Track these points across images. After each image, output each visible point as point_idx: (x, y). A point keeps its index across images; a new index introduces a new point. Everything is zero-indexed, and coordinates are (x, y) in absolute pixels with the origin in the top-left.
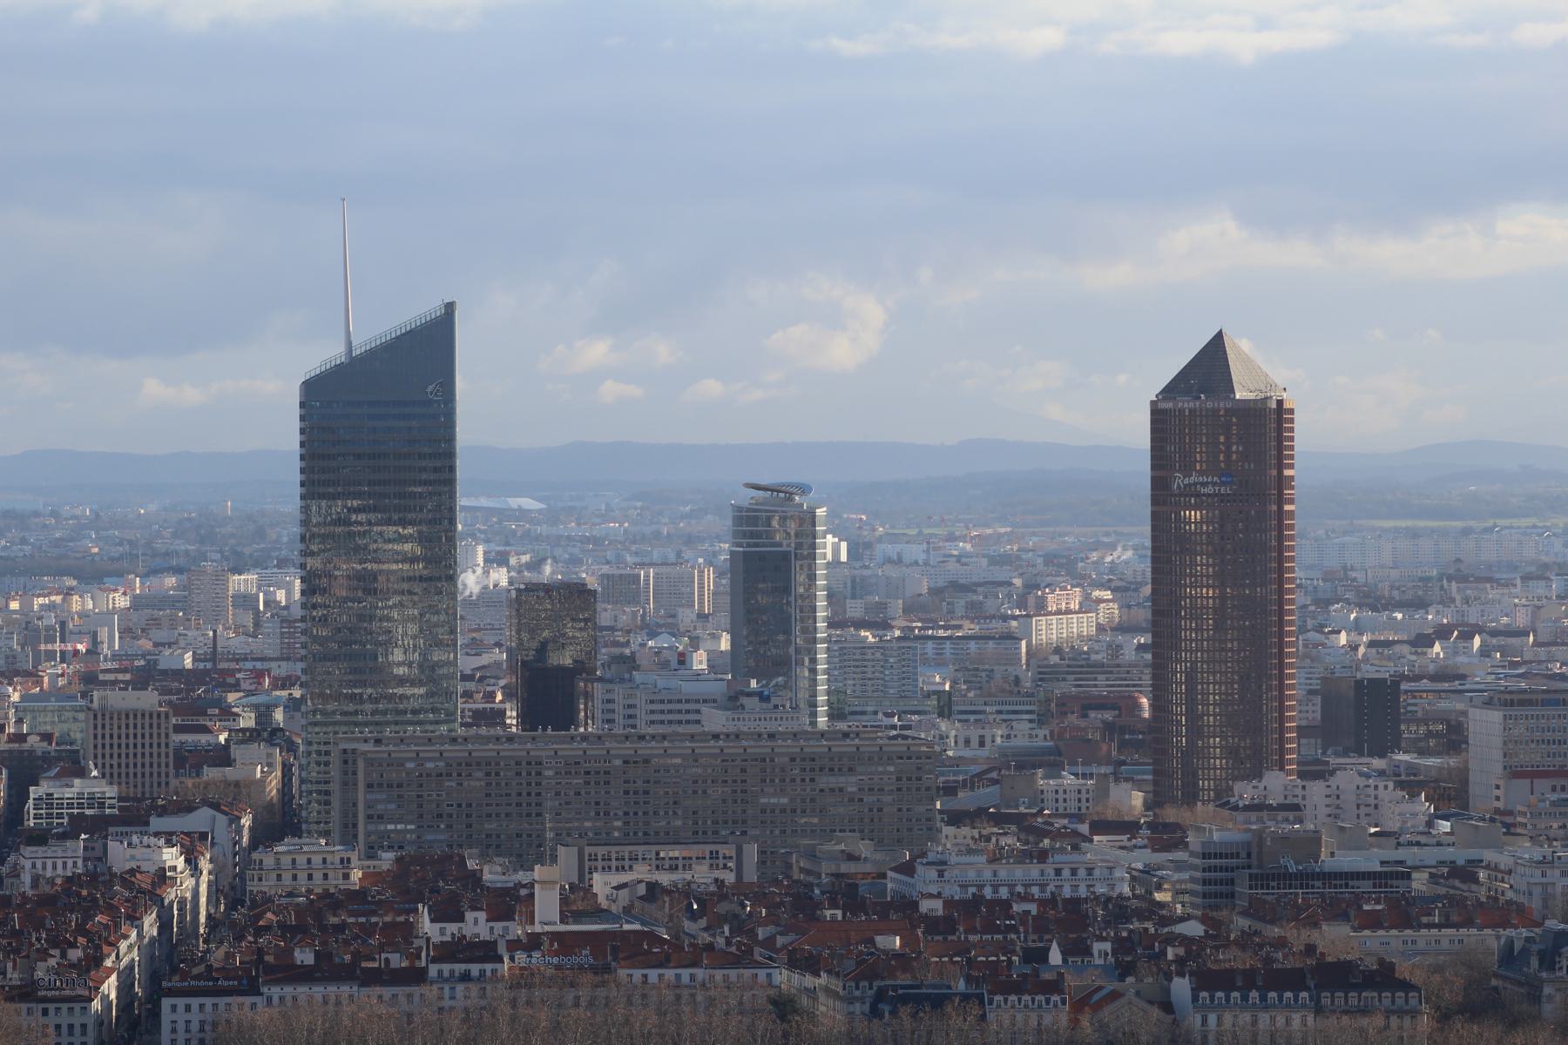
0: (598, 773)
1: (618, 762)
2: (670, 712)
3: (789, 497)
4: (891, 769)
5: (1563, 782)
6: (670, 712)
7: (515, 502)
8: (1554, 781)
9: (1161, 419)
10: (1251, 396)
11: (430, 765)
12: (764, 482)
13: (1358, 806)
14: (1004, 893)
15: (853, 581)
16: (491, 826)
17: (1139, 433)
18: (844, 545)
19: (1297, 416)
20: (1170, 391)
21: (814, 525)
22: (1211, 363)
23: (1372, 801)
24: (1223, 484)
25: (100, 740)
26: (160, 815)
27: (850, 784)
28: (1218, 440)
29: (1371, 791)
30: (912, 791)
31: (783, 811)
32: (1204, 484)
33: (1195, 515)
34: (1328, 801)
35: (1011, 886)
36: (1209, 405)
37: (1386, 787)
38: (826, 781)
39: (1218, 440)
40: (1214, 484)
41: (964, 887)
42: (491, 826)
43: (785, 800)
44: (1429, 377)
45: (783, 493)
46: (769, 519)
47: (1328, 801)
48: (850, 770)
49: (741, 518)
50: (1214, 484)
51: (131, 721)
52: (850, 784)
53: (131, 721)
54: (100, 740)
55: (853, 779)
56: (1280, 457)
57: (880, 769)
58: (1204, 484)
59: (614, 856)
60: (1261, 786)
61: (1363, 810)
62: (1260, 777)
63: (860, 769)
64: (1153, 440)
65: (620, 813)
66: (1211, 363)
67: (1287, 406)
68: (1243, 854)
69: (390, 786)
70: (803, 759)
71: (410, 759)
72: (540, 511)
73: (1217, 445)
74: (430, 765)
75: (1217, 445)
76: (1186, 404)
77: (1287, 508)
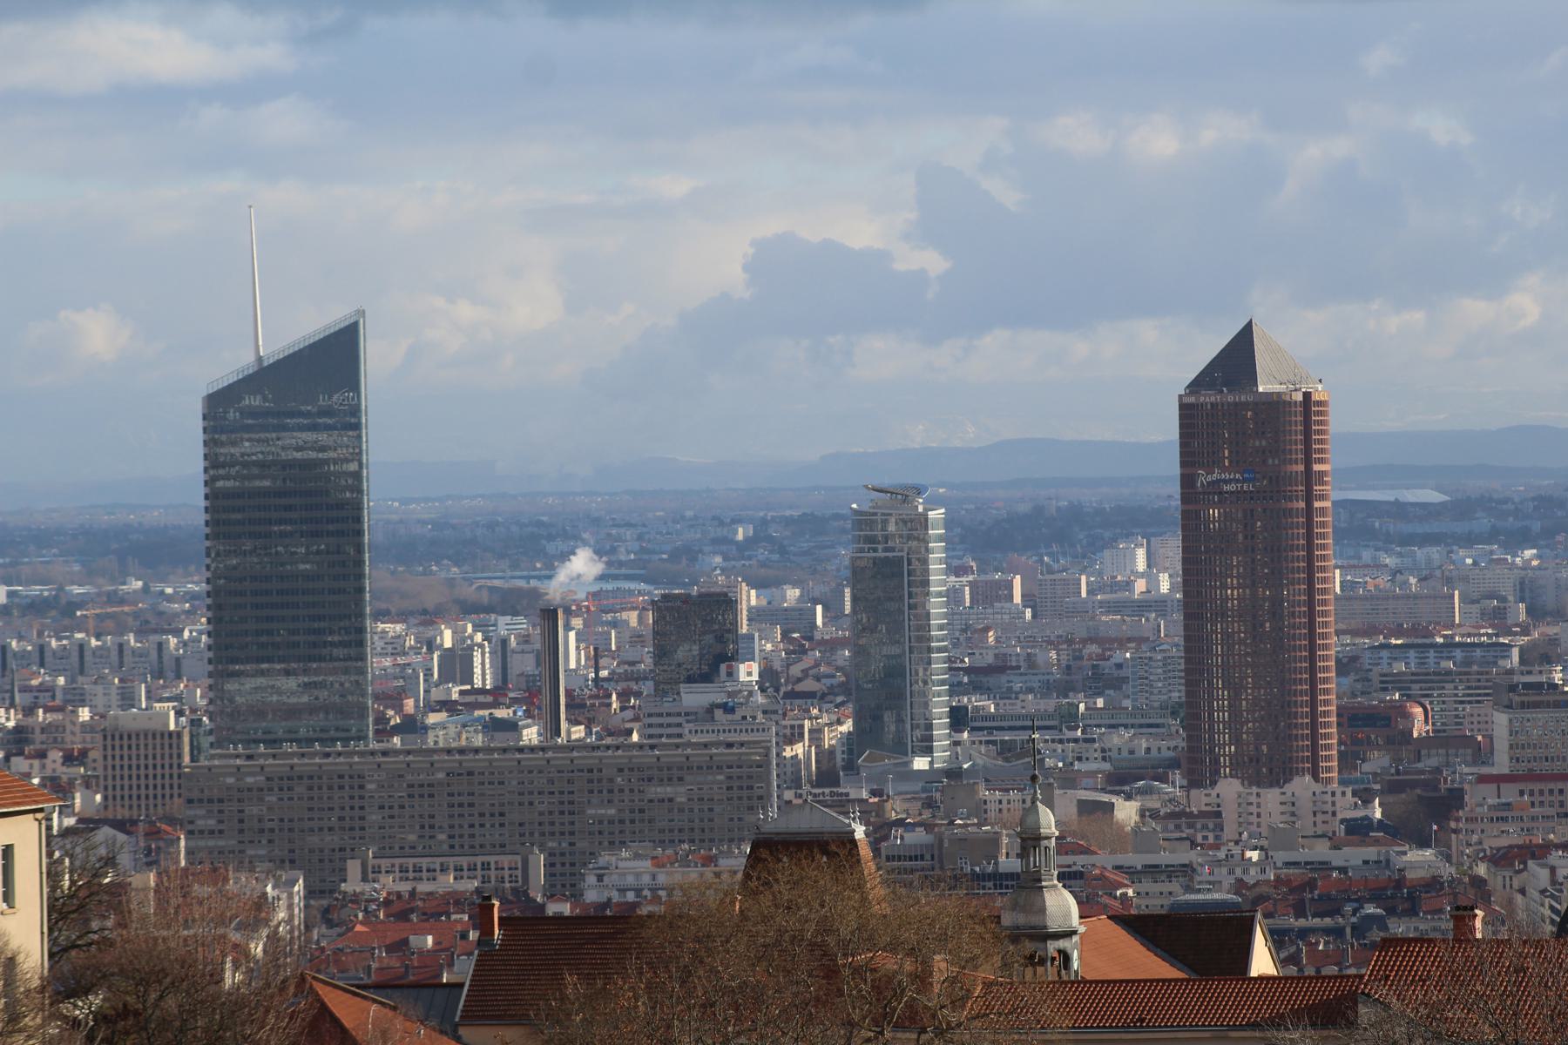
0: (422, 786)
1: (441, 775)
2: (669, 725)
4: (720, 777)
5: (1560, 785)
6: (669, 725)
8: (1521, 786)
9: (1189, 413)
11: (250, 780)
12: (877, 483)
13: (1315, 814)
15: (1522, 583)
16: (314, 840)
17: (1170, 431)
19: (1331, 409)
20: (1196, 385)
21: (926, 528)
23: (1329, 808)
24: (1245, 480)
25: (109, 752)
27: (680, 794)
28: (1243, 435)
29: (1328, 798)
31: (611, 822)
32: (1226, 482)
33: (1214, 513)
34: (1283, 809)
35: (638, 891)
36: (1230, 399)
37: (1343, 793)
39: (1243, 435)
40: (1237, 481)
41: (622, 891)
42: (314, 840)
43: (612, 811)
44: (1457, 360)
45: (904, 495)
46: (885, 522)
47: (1283, 809)
48: (680, 779)
49: (860, 522)
50: (1237, 481)
51: (142, 742)
52: (680, 794)
53: (142, 742)
54: (109, 752)
55: (682, 789)
57: (710, 778)
58: (1226, 482)
59: (493, 866)
60: (1214, 793)
61: (1320, 817)
62: (1214, 783)
63: (688, 778)
64: (1182, 435)
65: (445, 826)
67: (1316, 397)
68: (928, 857)
69: (210, 801)
70: (631, 770)
71: (231, 775)
72: (1442, 504)
73: (1243, 442)
74: (250, 780)
75: (1243, 442)
77: (1317, 504)
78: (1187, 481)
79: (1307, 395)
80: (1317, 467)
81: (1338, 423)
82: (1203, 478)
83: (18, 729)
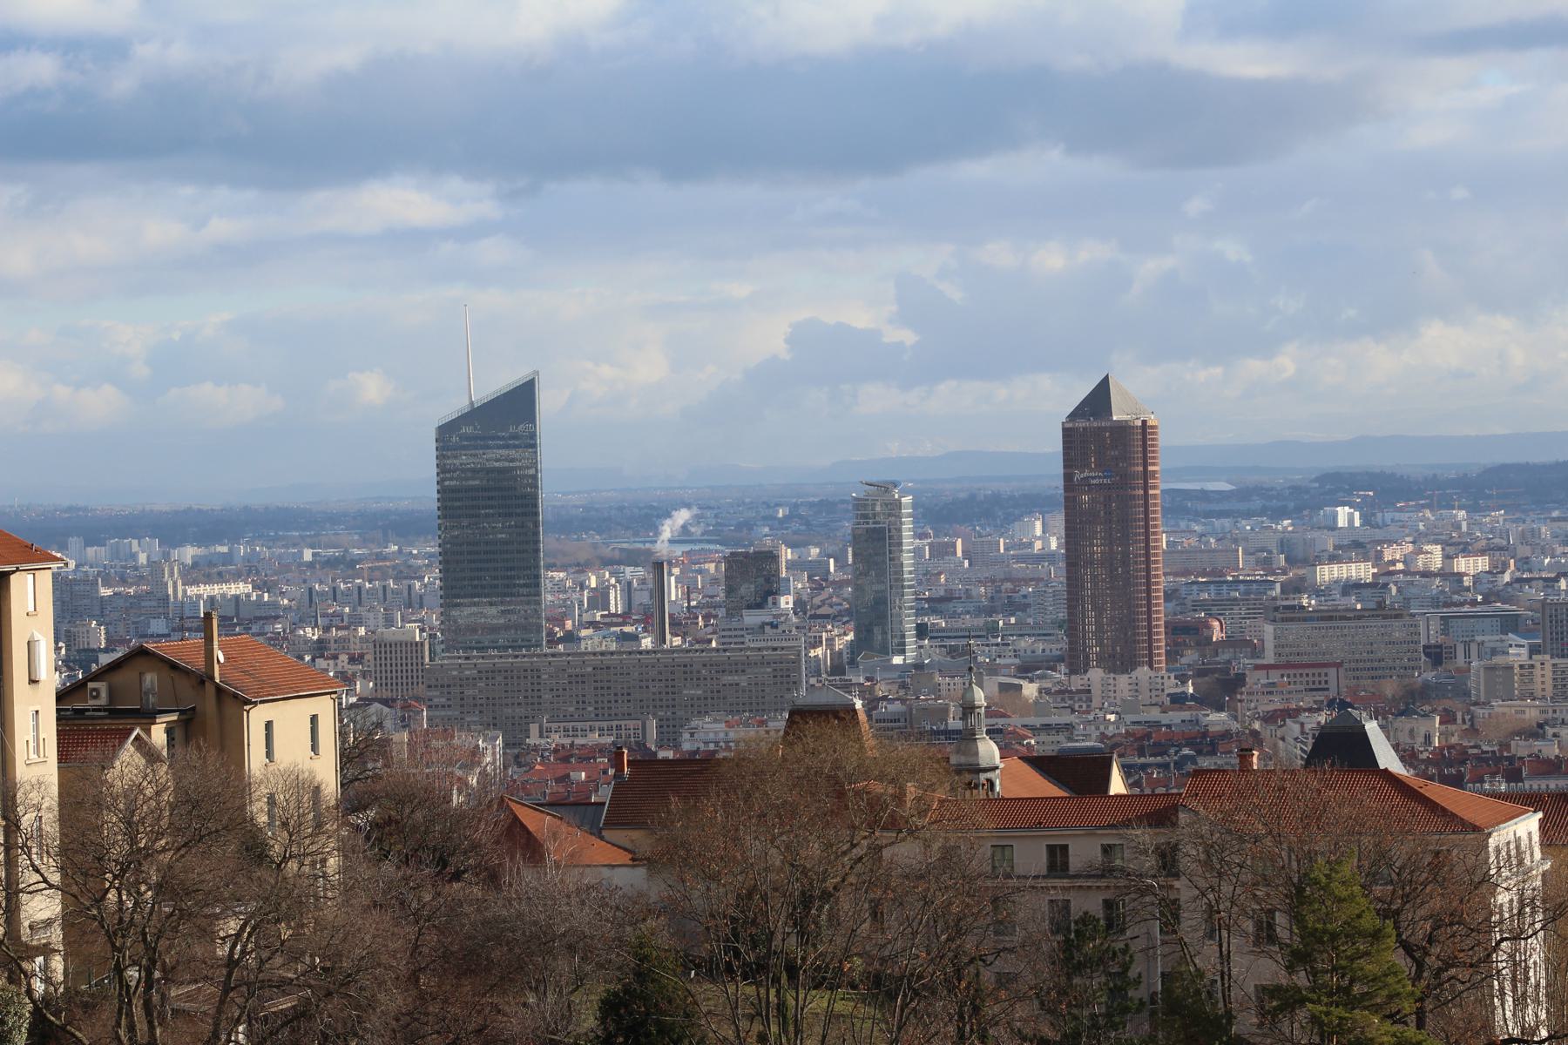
1: (590, 669)
3: (887, 490)
7: (1211, 486)
10: (1125, 417)
12: (874, 479)
14: (712, 747)
17: (1055, 444)
18: (1357, 515)
20: (1073, 416)
22: (1100, 398)
26: (1381, 727)
27: (743, 680)
28: (1104, 449)
30: (670, 685)
35: (717, 743)
38: (727, 679)
39: (1104, 449)
41: (706, 743)
45: (885, 487)
52: (743, 680)
56: (1145, 458)
62: (1086, 672)
66: (1100, 398)
76: (1081, 424)
78: (1068, 477)
79: (1144, 422)
80: (1151, 468)
81: (1165, 440)
82: (1078, 476)
83: (320, 641)
